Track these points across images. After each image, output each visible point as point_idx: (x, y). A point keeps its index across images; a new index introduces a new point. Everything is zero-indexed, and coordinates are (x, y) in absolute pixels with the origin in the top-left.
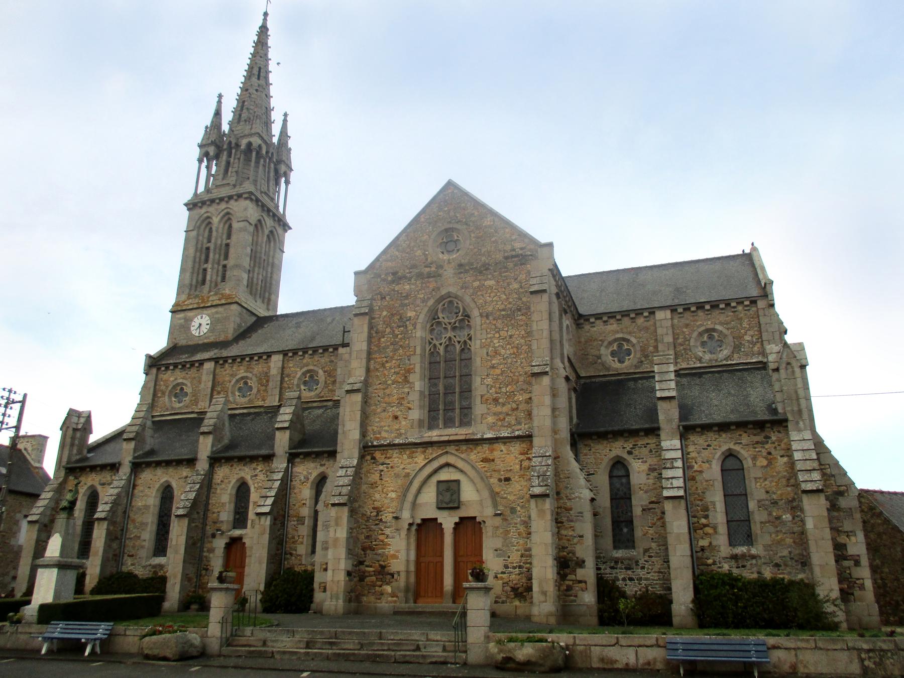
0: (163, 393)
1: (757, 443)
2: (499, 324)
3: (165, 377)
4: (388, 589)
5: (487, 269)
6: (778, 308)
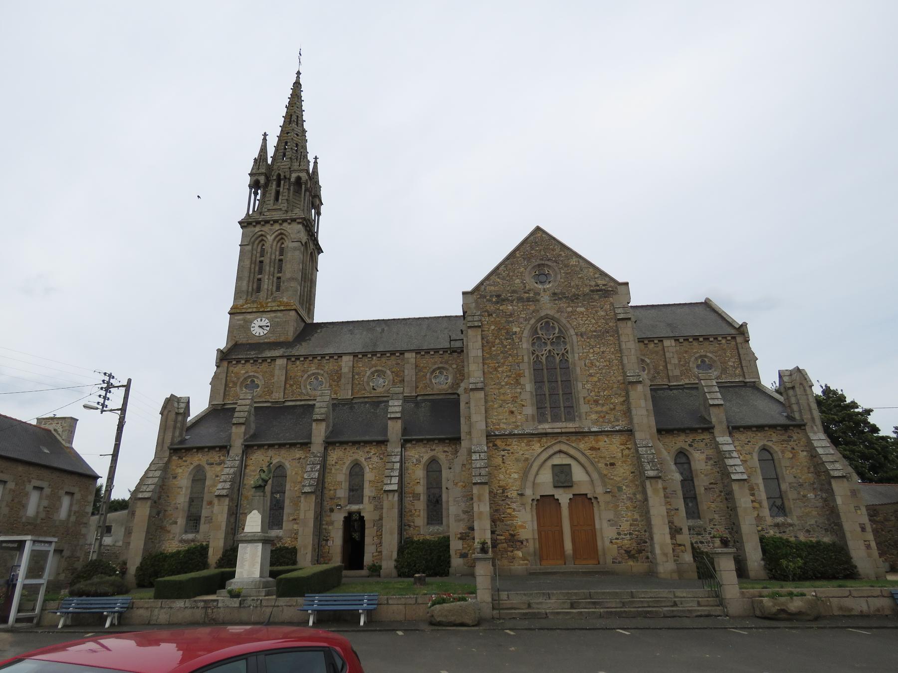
0: (235, 384)
1: (783, 441)
2: (592, 342)
3: (235, 370)
4: (520, 554)
5: (577, 299)
6: (752, 344)
